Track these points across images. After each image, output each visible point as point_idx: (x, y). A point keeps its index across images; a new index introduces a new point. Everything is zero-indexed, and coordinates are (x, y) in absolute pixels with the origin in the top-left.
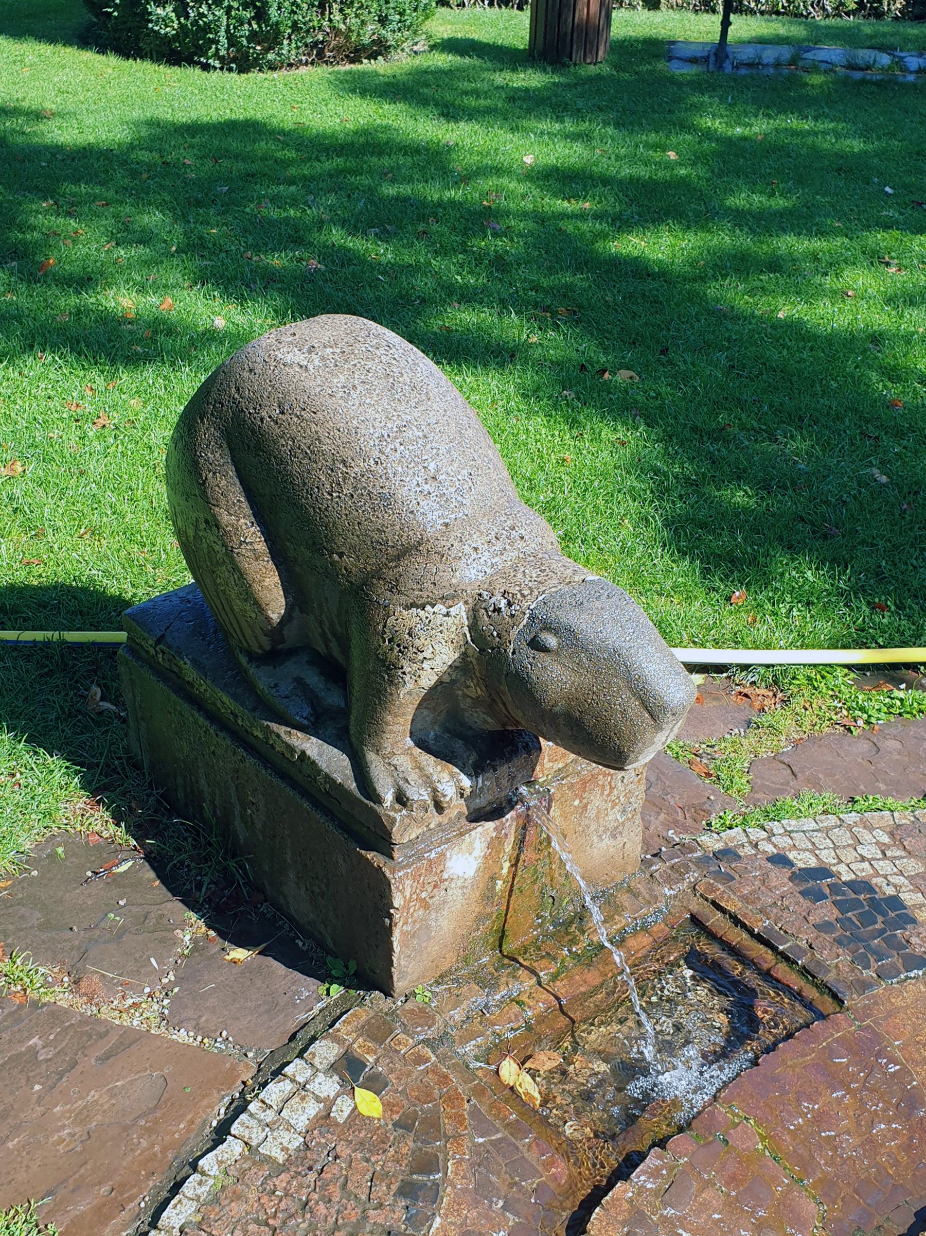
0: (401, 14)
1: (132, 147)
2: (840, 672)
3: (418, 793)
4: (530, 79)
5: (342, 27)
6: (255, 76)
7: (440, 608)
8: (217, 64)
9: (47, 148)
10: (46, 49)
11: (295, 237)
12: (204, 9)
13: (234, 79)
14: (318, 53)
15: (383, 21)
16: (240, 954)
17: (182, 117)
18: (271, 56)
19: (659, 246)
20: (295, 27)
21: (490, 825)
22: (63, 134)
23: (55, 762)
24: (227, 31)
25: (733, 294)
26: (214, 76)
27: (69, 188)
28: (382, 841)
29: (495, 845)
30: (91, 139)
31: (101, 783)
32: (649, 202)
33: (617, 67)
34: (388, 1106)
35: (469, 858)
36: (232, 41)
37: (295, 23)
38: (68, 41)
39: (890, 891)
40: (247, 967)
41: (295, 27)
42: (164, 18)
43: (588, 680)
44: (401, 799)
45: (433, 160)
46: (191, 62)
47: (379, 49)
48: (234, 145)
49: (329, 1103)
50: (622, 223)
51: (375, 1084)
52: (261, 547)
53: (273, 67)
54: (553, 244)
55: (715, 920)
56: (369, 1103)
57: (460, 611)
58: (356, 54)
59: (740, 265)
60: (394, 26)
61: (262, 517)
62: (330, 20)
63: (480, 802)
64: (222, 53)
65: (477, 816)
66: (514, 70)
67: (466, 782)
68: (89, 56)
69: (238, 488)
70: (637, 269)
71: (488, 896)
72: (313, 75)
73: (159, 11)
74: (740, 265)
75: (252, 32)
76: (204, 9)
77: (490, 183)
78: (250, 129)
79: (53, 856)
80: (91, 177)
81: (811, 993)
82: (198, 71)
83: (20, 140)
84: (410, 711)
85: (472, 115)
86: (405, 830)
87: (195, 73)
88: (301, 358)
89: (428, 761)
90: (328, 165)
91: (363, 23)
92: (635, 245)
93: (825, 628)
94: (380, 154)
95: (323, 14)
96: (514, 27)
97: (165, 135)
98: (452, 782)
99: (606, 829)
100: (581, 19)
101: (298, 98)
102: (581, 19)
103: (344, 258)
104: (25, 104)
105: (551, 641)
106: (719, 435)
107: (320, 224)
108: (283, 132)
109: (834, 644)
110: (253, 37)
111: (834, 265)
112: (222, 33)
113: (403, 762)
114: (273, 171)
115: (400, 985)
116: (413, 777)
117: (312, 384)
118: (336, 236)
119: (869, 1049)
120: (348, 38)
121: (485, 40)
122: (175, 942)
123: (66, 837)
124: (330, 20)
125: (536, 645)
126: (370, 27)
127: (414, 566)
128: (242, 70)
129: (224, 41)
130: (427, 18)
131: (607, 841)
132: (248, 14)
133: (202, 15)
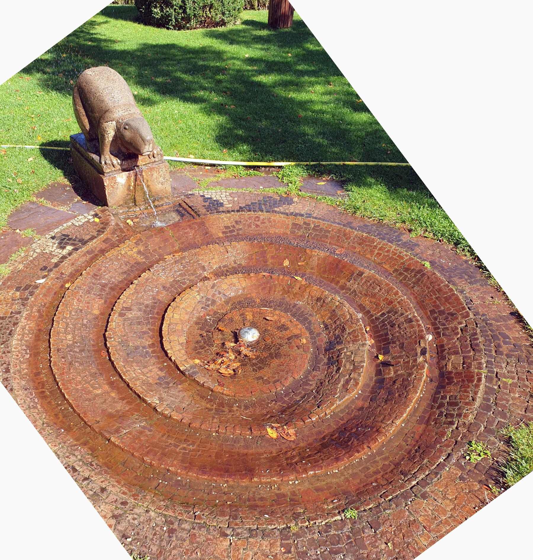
0: (230, 12)
1: (136, 51)
2: (241, 167)
3: (108, 162)
4: (264, 33)
5: (210, 16)
6: (182, 31)
7: (111, 122)
8: (172, 28)
9: (112, 51)
10: (124, 22)
11: (167, 74)
12: (168, 9)
13: (176, 32)
14: (203, 24)
15: (223, 14)
16: (85, 202)
17: (154, 43)
18: (188, 25)
19: (266, 79)
20: (195, 15)
21: (127, 173)
22: (118, 47)
23: (60, 171)
24: (175, 17)
25: (281, 92)
26: (170, 31)
27: (114, 61)
28: (103, 173)
29: (129, 178)
30: (126, 48)
31: (67, 174)
32: (270, 67)
33: (294, 29)
34: (100, 221)
35: (122, 178)
36: (176, 19)
37: (195, 14)
38: (131, 20)
39: (222, 202)
40: (86, 204)
41: (195, 15)
42: (157, 12)
43: (133, 135)
44: (105, 163)
45: (219, 55)
46: (164, 27)
47: (223, 23)
48: (165, 50)
49: (90, 219)
50: (260, 72)
51: (99, 218)
52: (84, 113)
53: (188, 29)
54: (240, 77)
55: (184, 205)
56: (97, 220)
57: (114, 123)
58: (217, 24)
59: (286, 84)
60: (227, 15)
61: (84, 107)
62: (206, 14)
63: (124, 167)
64: (173, 24)
65: (124, 170)
66: (260, 30)
67: (119, 161)
68: (136, 25)
69: (80, 101)
70: (260, 84)
71: (129, 189)
72: (201, 31)
73: (155, 10)
74: (286, 84)
75: (182, 17)
76: (168, 9)
77: (231, 62)
78: (173, 46)
79: (54, 186)
80: (118, 58)
81: (192, 213)
82: (165, 29)
83: (106, 48)
84: (109, 146)
85: (238, 43)
86: (106, 169)
87: (164, 30)
88: (91, 73)
89: (112, 157)
90: (188, 56)
91: (216, 14)
92: (263, 79)
93: (240, 158)
94: (204, 53)
95: (203, 11)
96: (262, 15)
97: (146, 47)
98: (116, 161)
99: (159, 182)
100: (283, 13)
101: (192, 38)
102: (283, 13)
103: (178, 79)
104: (112, 39)
105: (127, 127)
106: (246, 120)
107: (176, 71)
108: (181, 48)
109: (241, 161)
110: (183, 19)
111: (312, 84)
112: (173, 18)
113: (107, 157)
114: (172, 58)
115: (109, 204)
116: (108, 159)
117: (91, 78)
118: (179, 74)
119: (203, 224)
120: (211, 19)
121: (257, 20)
122: (74, 200)
123: (58, 183)
124: (206, 14)
125: (125, 128)
126: (219, 16)
127: (107, 114)
128: (179, 30)
129: (174, 20)
130: (239, 13)
131: (160, 185)
132: (181, 11)
133: (167, 11)
